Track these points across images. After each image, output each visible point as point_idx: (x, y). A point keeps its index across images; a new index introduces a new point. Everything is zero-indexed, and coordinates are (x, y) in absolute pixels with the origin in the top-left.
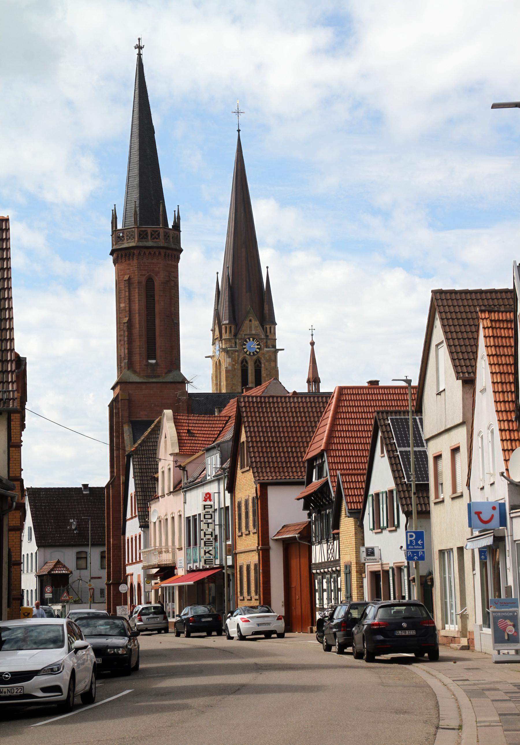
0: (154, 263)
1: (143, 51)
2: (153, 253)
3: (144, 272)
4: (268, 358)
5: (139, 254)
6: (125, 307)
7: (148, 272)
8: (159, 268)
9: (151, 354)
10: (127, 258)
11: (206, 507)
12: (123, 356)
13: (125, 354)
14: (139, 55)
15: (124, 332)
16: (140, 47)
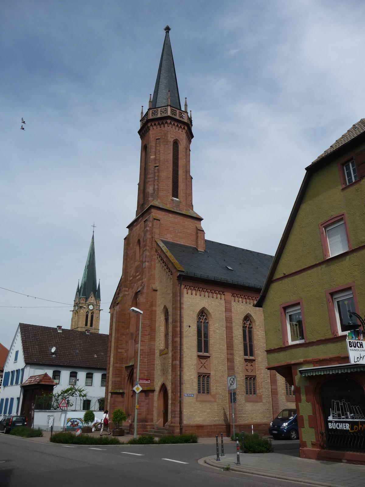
2: (179, 126)
5: (171, 123)
8: (183, 137)
10: (159, 126)
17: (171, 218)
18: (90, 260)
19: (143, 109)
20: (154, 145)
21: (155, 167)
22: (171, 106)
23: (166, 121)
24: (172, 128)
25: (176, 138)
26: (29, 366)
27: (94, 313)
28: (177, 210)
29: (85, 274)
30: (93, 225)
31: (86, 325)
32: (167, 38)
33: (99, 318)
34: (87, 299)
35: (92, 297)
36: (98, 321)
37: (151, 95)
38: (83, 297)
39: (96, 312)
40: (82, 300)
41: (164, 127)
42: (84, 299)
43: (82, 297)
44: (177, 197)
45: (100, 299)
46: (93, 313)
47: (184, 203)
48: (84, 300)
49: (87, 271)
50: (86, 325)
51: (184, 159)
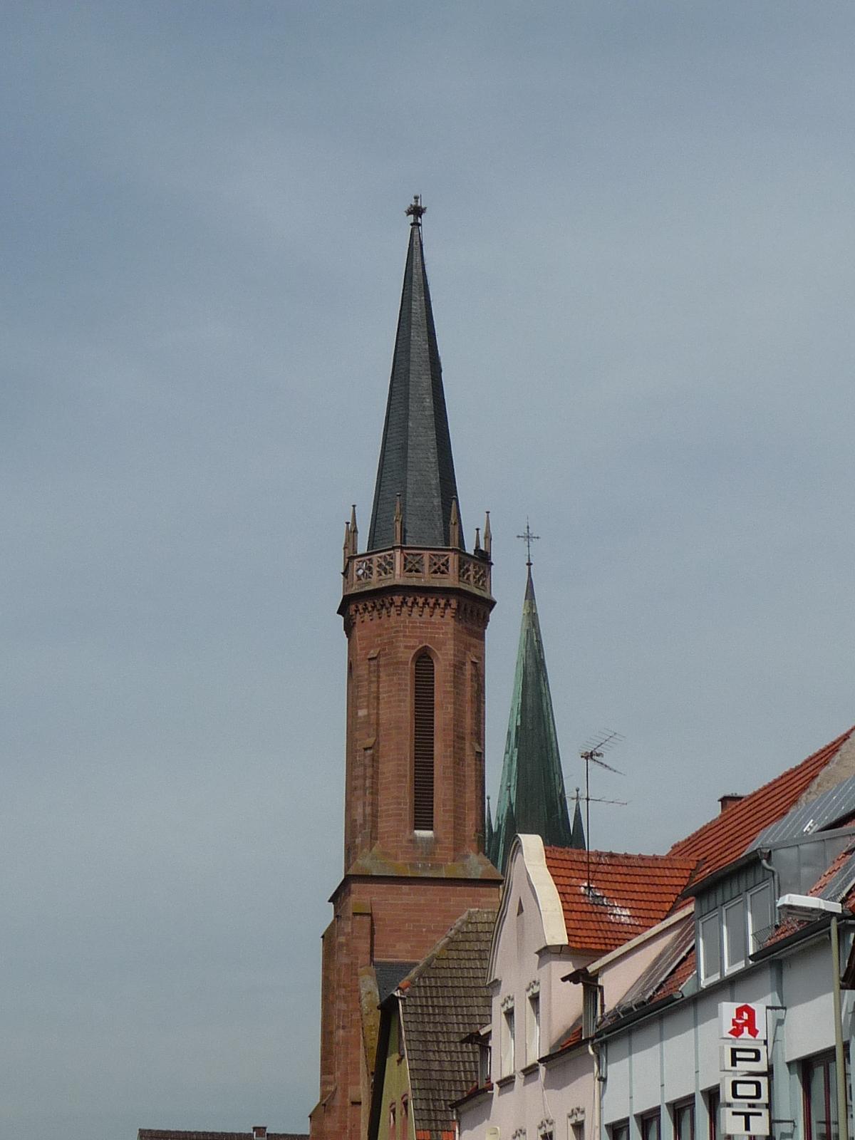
1: (424, 219)
3: (412, 642)
6: (369, 715)
7: (421, 642)
9: (423, 817)
10: (375, 613)
11: (739, 1055)
12: (360, 821)
13: (364, 815)
15: (365, 769)
17: (407, 896)
20: (366, 677)
21: (366, 749)
22: (402, 548)
23: (392, 599)
24: (410, 615)
25: (424, 645)
26: (727, 993)
28: (424, 868)
29: (510, 775)
32: (415, 250)
41: (389, 616)
44: (429, 825)
47: (448, 842)
51: (449, 706)
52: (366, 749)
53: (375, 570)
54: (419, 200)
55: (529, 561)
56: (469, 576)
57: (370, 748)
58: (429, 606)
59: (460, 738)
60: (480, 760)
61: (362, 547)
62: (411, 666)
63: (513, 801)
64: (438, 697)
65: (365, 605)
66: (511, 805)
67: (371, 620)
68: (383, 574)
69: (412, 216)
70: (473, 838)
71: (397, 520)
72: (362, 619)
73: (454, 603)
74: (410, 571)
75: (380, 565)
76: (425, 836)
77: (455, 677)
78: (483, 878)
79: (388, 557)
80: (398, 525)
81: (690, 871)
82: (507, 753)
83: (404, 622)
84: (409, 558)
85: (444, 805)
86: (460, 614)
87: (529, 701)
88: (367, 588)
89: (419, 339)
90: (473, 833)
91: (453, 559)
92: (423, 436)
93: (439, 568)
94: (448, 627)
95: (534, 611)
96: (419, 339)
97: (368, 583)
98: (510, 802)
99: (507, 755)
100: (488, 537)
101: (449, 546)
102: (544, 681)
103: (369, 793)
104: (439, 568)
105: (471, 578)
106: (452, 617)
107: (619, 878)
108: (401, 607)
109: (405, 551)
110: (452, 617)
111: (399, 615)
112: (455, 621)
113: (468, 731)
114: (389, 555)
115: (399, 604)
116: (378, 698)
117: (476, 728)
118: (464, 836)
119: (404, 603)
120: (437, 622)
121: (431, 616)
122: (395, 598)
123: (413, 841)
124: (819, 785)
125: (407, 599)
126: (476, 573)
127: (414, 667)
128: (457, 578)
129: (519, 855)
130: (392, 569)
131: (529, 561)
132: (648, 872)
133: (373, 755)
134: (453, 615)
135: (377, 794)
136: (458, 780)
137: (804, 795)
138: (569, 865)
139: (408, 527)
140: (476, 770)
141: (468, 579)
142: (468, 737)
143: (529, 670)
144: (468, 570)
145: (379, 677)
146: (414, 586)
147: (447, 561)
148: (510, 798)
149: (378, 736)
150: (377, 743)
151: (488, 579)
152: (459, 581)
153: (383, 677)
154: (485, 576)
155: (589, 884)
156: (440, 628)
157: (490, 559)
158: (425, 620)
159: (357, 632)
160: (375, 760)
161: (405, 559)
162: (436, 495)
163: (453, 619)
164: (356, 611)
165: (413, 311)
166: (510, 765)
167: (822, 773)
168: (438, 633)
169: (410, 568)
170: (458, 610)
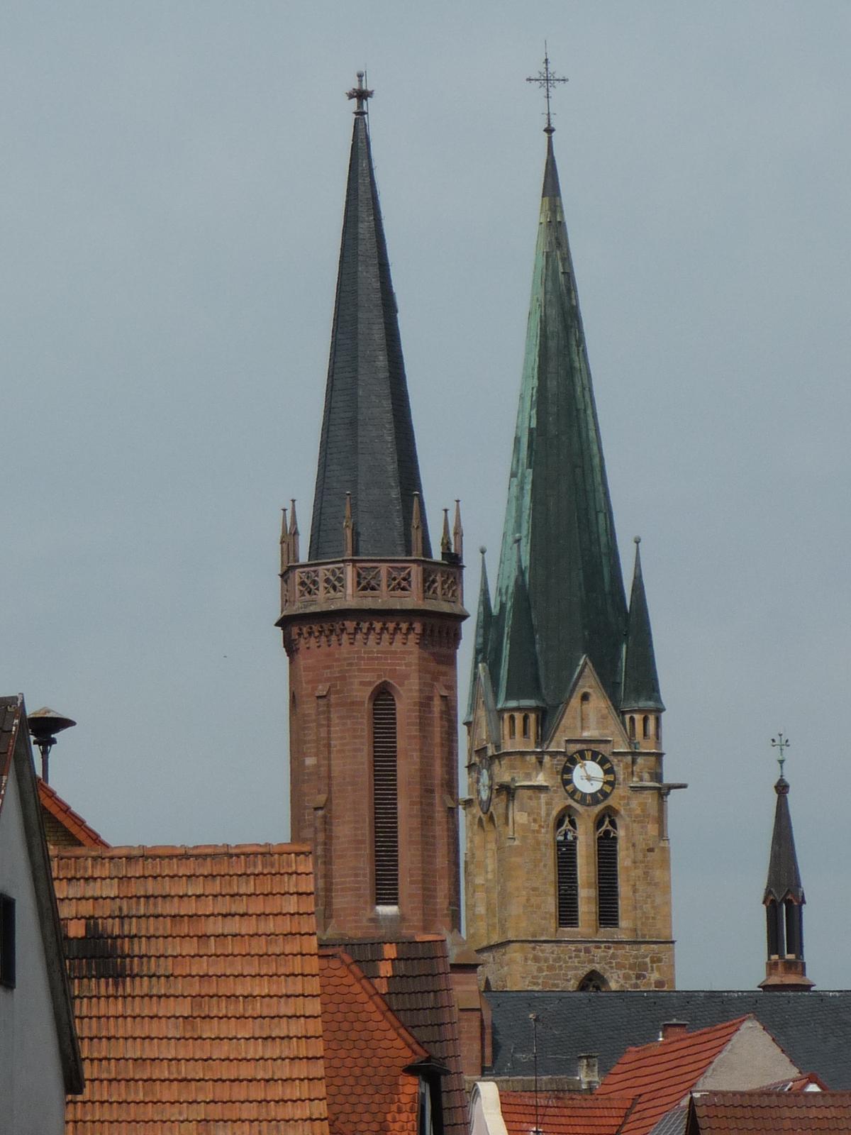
0: (395, 652)
1: (369, 105)
3: (369, 677)
4: (638, 812)
6: (318, 766)
7: (379, 677)
9: (385, 890)
10: (323, 639)
14: (360, 114)
15: (316, 832)
16: (361, 95)
18: (542, 390)
19: (297, 509)
20: (314, 717)
21: (316, 809)
22: (354, 561)
23: (343, 625)
24: (365, 644)
25: (383, 679)
27: (619, 822)
30: (536, 69)
31: (567, 913)
33: (665, 851)
34: (546, 719)
35: (585, 697)
36: (657, 873)
37: (284, 510)
38: (518, 709)
39: (629, 805)
40: (512, 733)
41: (340, 645)
42: (526, 719)
43: (512, 704)
45: (658, 700)
46: (607, 817)
48: (525, 732)
49: (528, 487)
50: (567, 913)
52: (316, 809)
53: (322, 585)
54: (364, 78)
55: (549, 125)
56: (436, 588)
57: (321, 808)
58: (388, 632)
59: (428, 791)
60: (453, 817)
61: (303, 557)
62: (367, 706)
63: (526, 561)
64: (401, 743)
65: (311, 628)
66: (521, 572)
67: (319, 647)
68: (332, 591)
69: (356, 99)
70: (446, 912)
71: (347, 526)
72: (308, 646)
73: (418, 627)
74: (364, 589)
75: (327, 581)
76: (389, 914)
77: (420, 718)
78: (459, 962)
79: (337, 570)
80: (349, 533)
81: (626, 1110)
82: (513, 475)
83: (357, 652)
84: (364, 574)
85: (411, 876)
86: (426, 639)
87: (552, 384)
88: (313, 609)
89: (367, 275)
90: (446, 904)
91: (416, 572)
92: (378, 408)
93: (399, 584)
94: (411, 656)
95: (559, 220)
96: (367, 275)
97: (313, 602)
98: (520, 567)
99: (515, 481)
100: (458, 533)
101: (411, 556)
102: (578, 346)
103: (321, 863)
104: (399, 584)
105: (439, 590)
106: (417, 643)
107: (563, 1120)
108: (355, 634)
109: (358, 565)
110: (417, 643)
111: (352, 644)
112: (420, 648)
113: (437, 782)
114: (339, 569)
115: (352, 631)
116: (329, 746)
117: (447, 777)
118: (435, 910)
119: (357, 629)
120: (399, 650)
121: (391, 643)
122: (347, 623)
123: (375, 920)
124: (714, 1070)
125: (362, 624)
126: (444, 582)
127: (371, 707)
128: (421, 595)
129: (478, 1099)
130: (342, 586)
131: (549, 125)
132: (588, 1112)
133: (325, 817)
134: (418, 641)
135: (331, 864)
136: (427, 844)
137: (702, 1078)
138: (521, 1109)
139: (362, 530)
140: (448, 830)
141: (434, 592)
142: (438, 790)
143: (550, 328)
144: (434, 581)
145: (329, 719)
146: (370, 609)
147: (409, 574)
148: (520, 560)
149: (330, 792)
150: (329, 800)
151: (459, 589)
152: (425, 598)
153: (334, 716)
154: (456, 584)
155: (537, 1129)
156: (402, 657)
157: (462, 562)
158: (384, 650)
159: (302, 661)
160: (327, 821)
161: (359, 575)
162: (393, 484)
163: (417, 646)
164: (300, 635)
165: (361, 237)
166: (520, 498)
167: (716, 1061)
168: (399, 665)
169: (365, 585)
170: (422, 635)
